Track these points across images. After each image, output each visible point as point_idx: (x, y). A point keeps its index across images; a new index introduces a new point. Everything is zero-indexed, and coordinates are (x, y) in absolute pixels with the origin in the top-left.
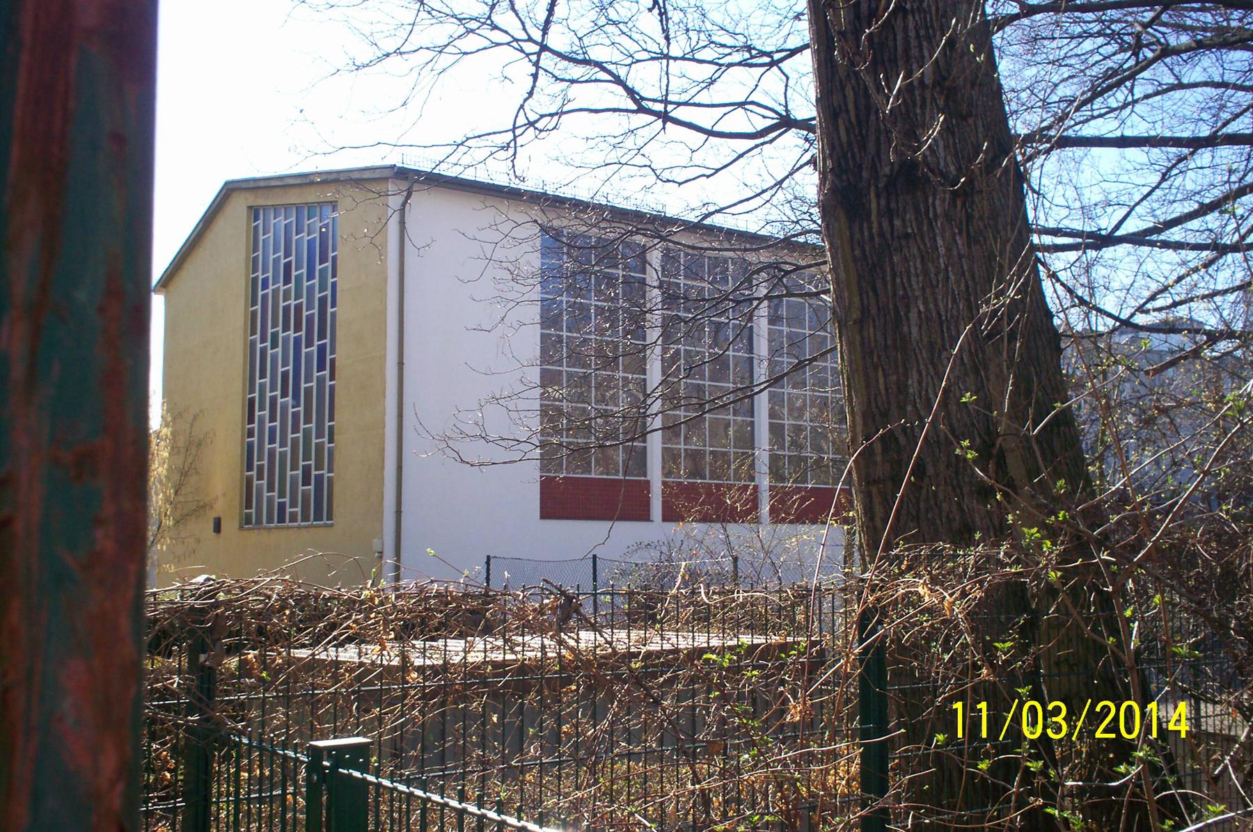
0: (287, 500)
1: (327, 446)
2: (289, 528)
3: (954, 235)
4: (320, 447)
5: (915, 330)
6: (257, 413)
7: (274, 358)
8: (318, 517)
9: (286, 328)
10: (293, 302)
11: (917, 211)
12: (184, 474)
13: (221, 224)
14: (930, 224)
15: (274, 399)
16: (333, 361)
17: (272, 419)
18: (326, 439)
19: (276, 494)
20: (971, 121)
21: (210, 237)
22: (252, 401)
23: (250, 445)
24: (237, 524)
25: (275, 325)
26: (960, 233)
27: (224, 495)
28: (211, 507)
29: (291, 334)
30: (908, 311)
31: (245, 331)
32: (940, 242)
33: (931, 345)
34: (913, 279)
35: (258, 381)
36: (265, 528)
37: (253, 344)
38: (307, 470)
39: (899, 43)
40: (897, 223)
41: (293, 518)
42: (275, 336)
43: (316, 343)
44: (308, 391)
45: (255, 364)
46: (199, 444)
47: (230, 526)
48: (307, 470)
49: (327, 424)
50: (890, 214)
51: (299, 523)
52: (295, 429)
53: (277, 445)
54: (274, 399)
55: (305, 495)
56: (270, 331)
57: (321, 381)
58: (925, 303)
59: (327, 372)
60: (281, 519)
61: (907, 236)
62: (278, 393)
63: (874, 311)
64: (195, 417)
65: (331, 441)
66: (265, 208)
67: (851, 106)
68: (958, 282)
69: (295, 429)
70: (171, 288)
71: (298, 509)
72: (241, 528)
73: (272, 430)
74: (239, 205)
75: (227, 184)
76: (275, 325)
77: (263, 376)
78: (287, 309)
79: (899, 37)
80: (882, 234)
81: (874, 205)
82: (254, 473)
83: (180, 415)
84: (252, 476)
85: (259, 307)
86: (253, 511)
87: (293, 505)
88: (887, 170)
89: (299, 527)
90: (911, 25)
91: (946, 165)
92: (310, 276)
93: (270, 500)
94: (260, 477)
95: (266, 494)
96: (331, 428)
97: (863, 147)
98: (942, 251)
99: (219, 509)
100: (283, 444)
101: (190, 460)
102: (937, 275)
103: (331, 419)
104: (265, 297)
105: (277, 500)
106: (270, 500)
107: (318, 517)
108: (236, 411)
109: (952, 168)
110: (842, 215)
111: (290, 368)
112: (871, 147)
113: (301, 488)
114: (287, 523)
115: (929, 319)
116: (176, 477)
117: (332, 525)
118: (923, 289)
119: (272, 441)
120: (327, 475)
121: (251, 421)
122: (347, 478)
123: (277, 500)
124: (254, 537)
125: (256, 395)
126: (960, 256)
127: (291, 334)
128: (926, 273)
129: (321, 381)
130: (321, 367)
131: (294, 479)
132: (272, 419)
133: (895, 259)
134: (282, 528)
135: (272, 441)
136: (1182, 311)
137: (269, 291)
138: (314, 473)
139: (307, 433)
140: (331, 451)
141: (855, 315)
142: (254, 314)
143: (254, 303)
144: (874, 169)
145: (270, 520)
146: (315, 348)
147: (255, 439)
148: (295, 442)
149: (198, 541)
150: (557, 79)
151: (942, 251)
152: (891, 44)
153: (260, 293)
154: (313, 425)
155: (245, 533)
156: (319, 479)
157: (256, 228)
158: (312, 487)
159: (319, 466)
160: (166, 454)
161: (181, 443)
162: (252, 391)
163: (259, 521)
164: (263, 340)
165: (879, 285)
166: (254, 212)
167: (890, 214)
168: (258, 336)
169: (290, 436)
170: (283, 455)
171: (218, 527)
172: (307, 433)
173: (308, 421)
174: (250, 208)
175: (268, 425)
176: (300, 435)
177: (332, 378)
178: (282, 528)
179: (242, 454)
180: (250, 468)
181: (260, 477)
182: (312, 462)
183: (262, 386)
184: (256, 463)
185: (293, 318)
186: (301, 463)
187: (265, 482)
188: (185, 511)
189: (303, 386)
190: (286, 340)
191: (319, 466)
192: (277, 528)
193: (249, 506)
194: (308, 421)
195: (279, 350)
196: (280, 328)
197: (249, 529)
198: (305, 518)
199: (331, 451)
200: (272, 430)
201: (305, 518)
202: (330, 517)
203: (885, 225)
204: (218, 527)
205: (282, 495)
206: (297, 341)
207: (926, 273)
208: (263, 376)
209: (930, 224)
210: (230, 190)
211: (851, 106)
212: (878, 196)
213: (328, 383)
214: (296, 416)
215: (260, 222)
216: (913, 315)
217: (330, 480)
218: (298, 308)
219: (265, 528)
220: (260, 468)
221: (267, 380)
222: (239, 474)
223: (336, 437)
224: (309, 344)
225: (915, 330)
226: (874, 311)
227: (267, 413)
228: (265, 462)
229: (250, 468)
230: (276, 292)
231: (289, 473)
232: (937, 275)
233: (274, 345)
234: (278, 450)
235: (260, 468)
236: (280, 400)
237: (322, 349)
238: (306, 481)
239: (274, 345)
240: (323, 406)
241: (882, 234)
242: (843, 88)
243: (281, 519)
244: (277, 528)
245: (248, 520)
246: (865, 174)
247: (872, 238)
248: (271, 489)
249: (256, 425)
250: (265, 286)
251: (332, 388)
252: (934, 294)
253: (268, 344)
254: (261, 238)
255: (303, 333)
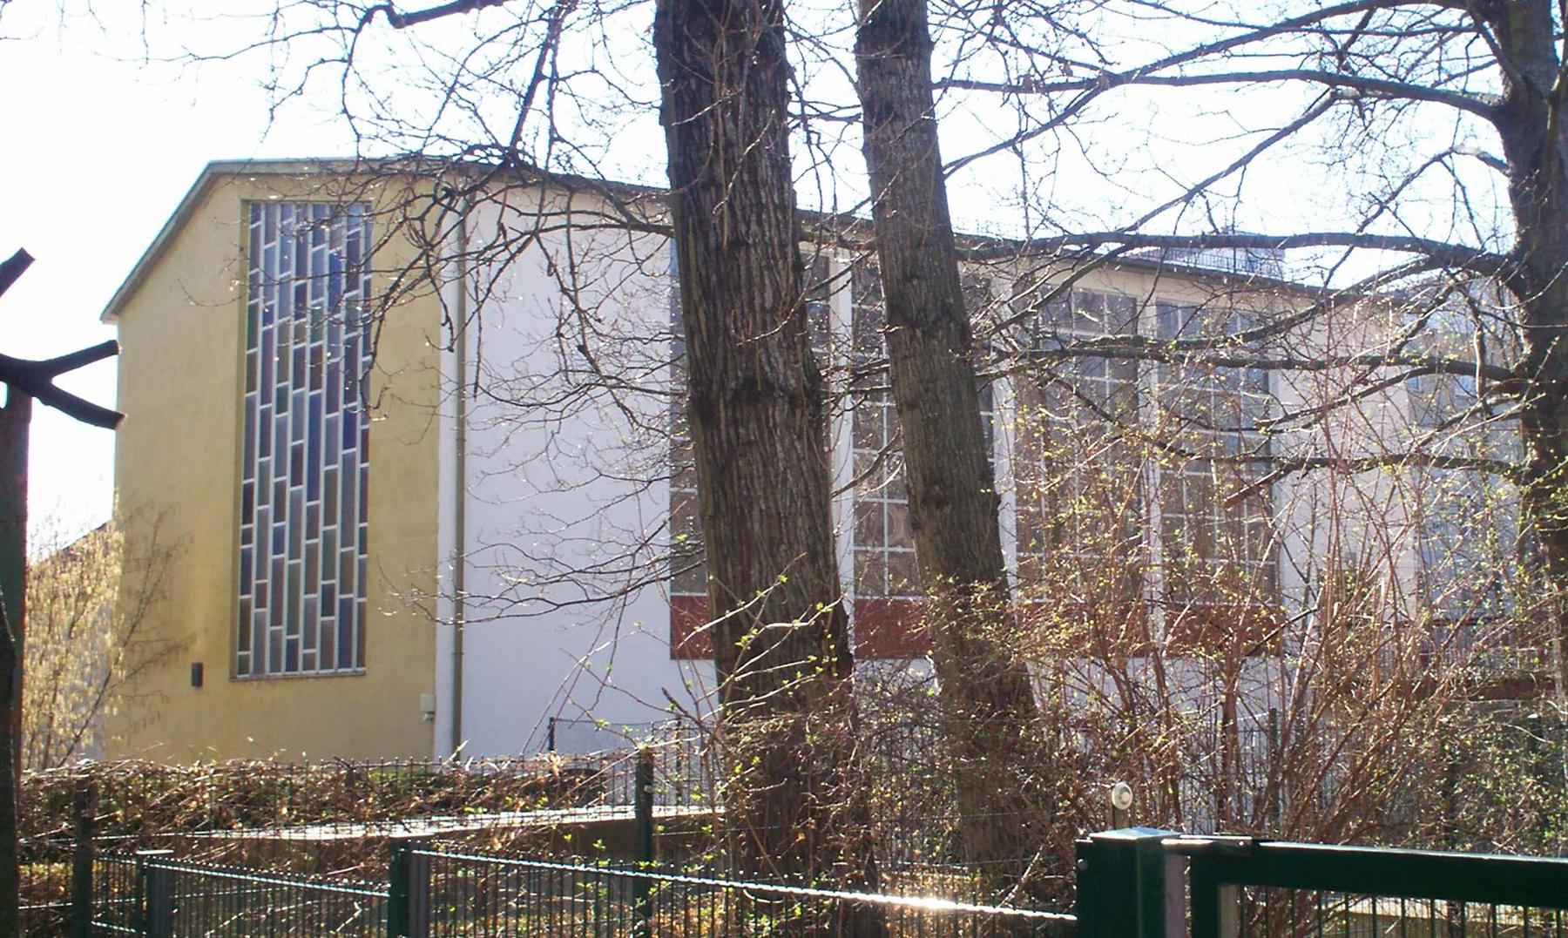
0: (300, 636)
1: (357, 557)
2: (302, 678)
3: (793, 443)
4: (347, 559)
5: (757, 526)
6: (256, 508)
7: (281, 426)
8: (344, 662)
9: (298, 383)
10: (308, 345)
11: (758, 420)
12: (146, 600)
13: (202, 222)
14: (770, 432)
15: (280, 488)
16: (365, 434)
17: (279, 516)
18: (356, 548)
19: (283, 628)
20: (915, 282)
21: (186, 242)
22: (248, 490)
23: (246, 557)
24: (227, 674)
25: (282, 377)
26: (799, 438)
27: (206, 630)
28: (186, 649)
29: (306, 392)
30: (751, 509)
31: (239, 387)
32: (779, 448)
33: (771, 540)
34: (756, 482)
35: (258, 460)
36: (268, 679)
37: (250, 404)
38: (328, 593)
39: (743, 273)
40: (742, 431)
41: (309, 663)
42: (282, 393)
43: (342, 406)
44: (331, 476)
45: (254, 435)
46: (168, 555)
47: (216, 676)
48: (328, 593)
49: (358, 525)
50: (735, 423)
51: (317, 670)
52: (312, 533)
53: (285, 555)
54: (280, 488)
55: (327, 629)
56: (275, 386)
57: (348, 462)
58: (766, 502)
59: (357, 450)
60: (292, 665)
61: (750, 443)
62: (287, 478)
63: (723, 508)
64: (160, 518)
65: (363, 550)
66: (269, 205)
67: (703, 327)
68: (796, 483)
69: (312, 533)
70: (129, 314)
71: (316, 651)
72: (233, 678)
73: (279, 534)
74: (228, 201)
75: (211, 165)
76: (282, 377)
77: (265, 451)
78: (299, 354)
79: (742, 268)
80: (729, 441)
81: (722, 415)
82: (252, 596)
83: (140, 511)
84: (249, 601)
85: (258, 350)
86: (251, 653)
87: (309, 643)
88: (733, 385)
89: (317, 677)
90: (753, 257)
91: (786, 380)
92: (334, 308)
93: (275, 637)
94: (261, 603)
95: (269, 629)
96: (363, 531)
97: (713, 361)
98: (781, 455)
99: (199, 650)
100: (294, 554)
101: (154, 580)
102: (776, 476)
103: (363, 518)
104: (267, 335)
105: (285, 637)
106: (275, 637)
107: (344, 662)
108: (226, 503)
109: (792, 382)
110: (698, 421)
111: (305, 441)
112: (720, 366)
113: (320, 619)
114: (300, 671)
115: (769, 516)
116: (133, 605)
117: (363, 674)
118: (764, 490)
119: (278, 549)
120: (357, 600)
121: (247, 518)
122: (385, 612)
123: (285, 637)
124: (250, 692)
125: (255, 480)
126: (799, 460)
127: (306, 392)
128: (766, 474)
129: (348, 462)
130: (349, 442)
131: (310, 607)
132: (279, 516)
133: (740, 463)
134: (293, 678)
135: (278, 549)
136: (1406, 413)
137: (274, 326)
138: (338, 597)
139: (329, 538)
140: (362, 564)
141: (710, 512)
142: (252, 359)
143: (252, 343)
144: (722, 384)
145: (275, 667)
146: (339, 415)
147: (254, 546)
148: (311, 551)
149: (166, 699)
150: (521, 214)
151: (781, 455)
152: (735, 273)
153: (261, 329)
154: (337, 527)
155: (240, 687)
156: (347, 605)
157: (255, 232)
158: (335, 618)
159: (346, 588)
160: (117, 570)
161: (141, 552)
162: (248, 473)
163: (259, 667)
164: (265, 399)
165: (727, 485)
166: (253, 208)
167: (735, 423)
168: (257, 393)
169: (304, 542)
170: (294, 570)
171: (198, 678)
172: (329, 538)
173: (330, 520)
174: (246, 202)
175: (272, 525)
176: (319, 541)
177: (364, 459)
178: (293, 678)
179: (234, 571)
180: (245, 589)
181: (261, 603)
182: (336, 581)
183: (264, 469)
184: (254, 582)
185: (305, 368)
186: (321, 583)
187: (267, 610)
188: (148, 655)
189: (323, 468)
190: (298, 400)
191: (346, 588)
192: (285, 678)
193: (244, 645)
194: (330, 520)
195: (289, 414)
196: (290, 383)
197: (245, 680)
198: (326, 663)
199: (362, 564)
200: (279, 534)
201: (326, 663)
202: (361, 663)
203: (732, 433)
204: (198, 678)
205: (292, 629)
206: (315, 402)
207: (766, 474)
208: (265, 451)
209: (770, 432)
210: (215, 176)
211: (703, 327)
212: (726, 406)
213: (359, 466)
214: (312, 512)
215: (261, 223)
216: (756, 513)
217: (361, 607)
218: (317, 353)
219: (268, 679)
220: (261, 590)
221: (271, 458)
222: (229, 597)
223: (369, 545)
224: (332, 407)
225: (757, 526)
226: (723, 508)
227: (270, 507)
228: (268, 581)
229: (245, 589)
230: (283, 329)
231: (303, 597)
232: (776, 476)
233: (281, 408)
234: (288, 562)
235: (261, 590)
236: (289, 489)
237: (349, 419)
238: (327, 610)
239: (281, 408)
240: (352, 498)
241: (729, 441)
242: (696, 310)
243: (292, 665)
244: (285, 678)
245: (242, 667)
246: (715, 387)
247: (721, 443)
248: (276, 620)
249: (254, 525)
250: (268, 319)
251: (364, 472)
252: (773, 493)
253: (273, 405)
254: (263, 247)
255: (323, 391)
